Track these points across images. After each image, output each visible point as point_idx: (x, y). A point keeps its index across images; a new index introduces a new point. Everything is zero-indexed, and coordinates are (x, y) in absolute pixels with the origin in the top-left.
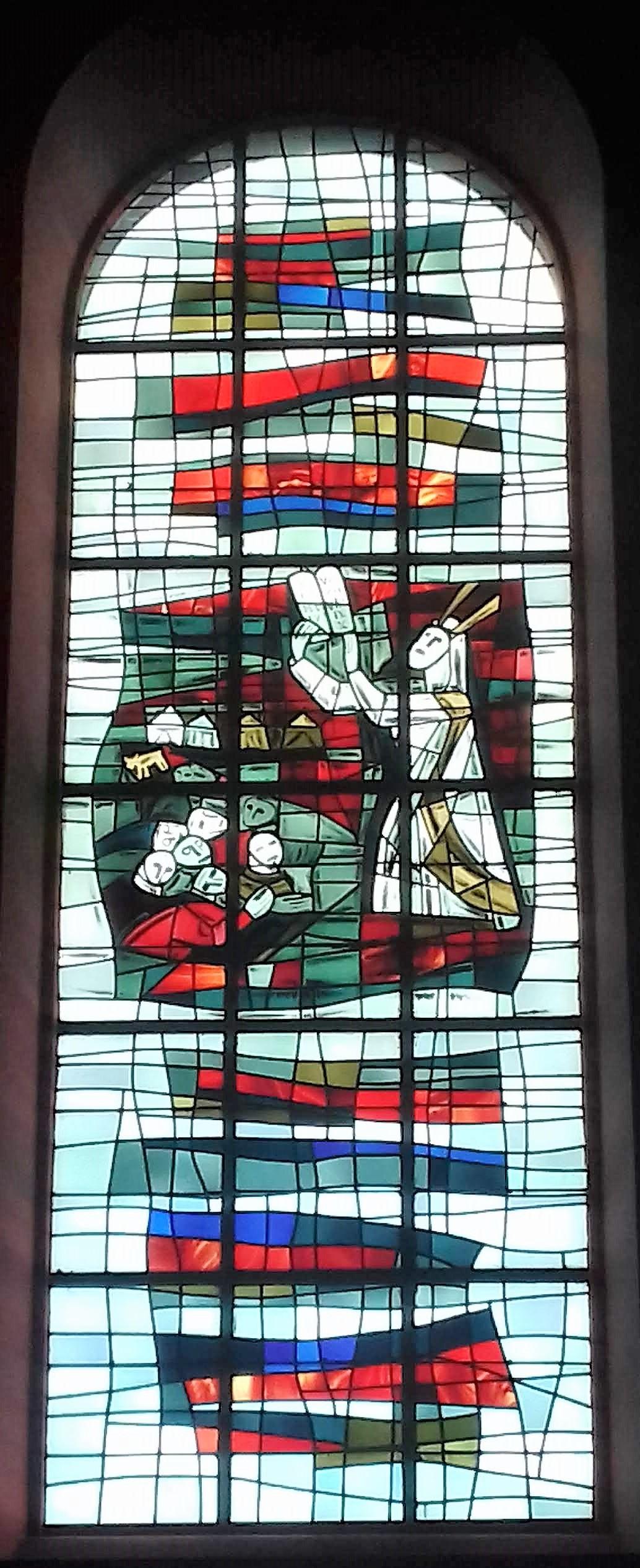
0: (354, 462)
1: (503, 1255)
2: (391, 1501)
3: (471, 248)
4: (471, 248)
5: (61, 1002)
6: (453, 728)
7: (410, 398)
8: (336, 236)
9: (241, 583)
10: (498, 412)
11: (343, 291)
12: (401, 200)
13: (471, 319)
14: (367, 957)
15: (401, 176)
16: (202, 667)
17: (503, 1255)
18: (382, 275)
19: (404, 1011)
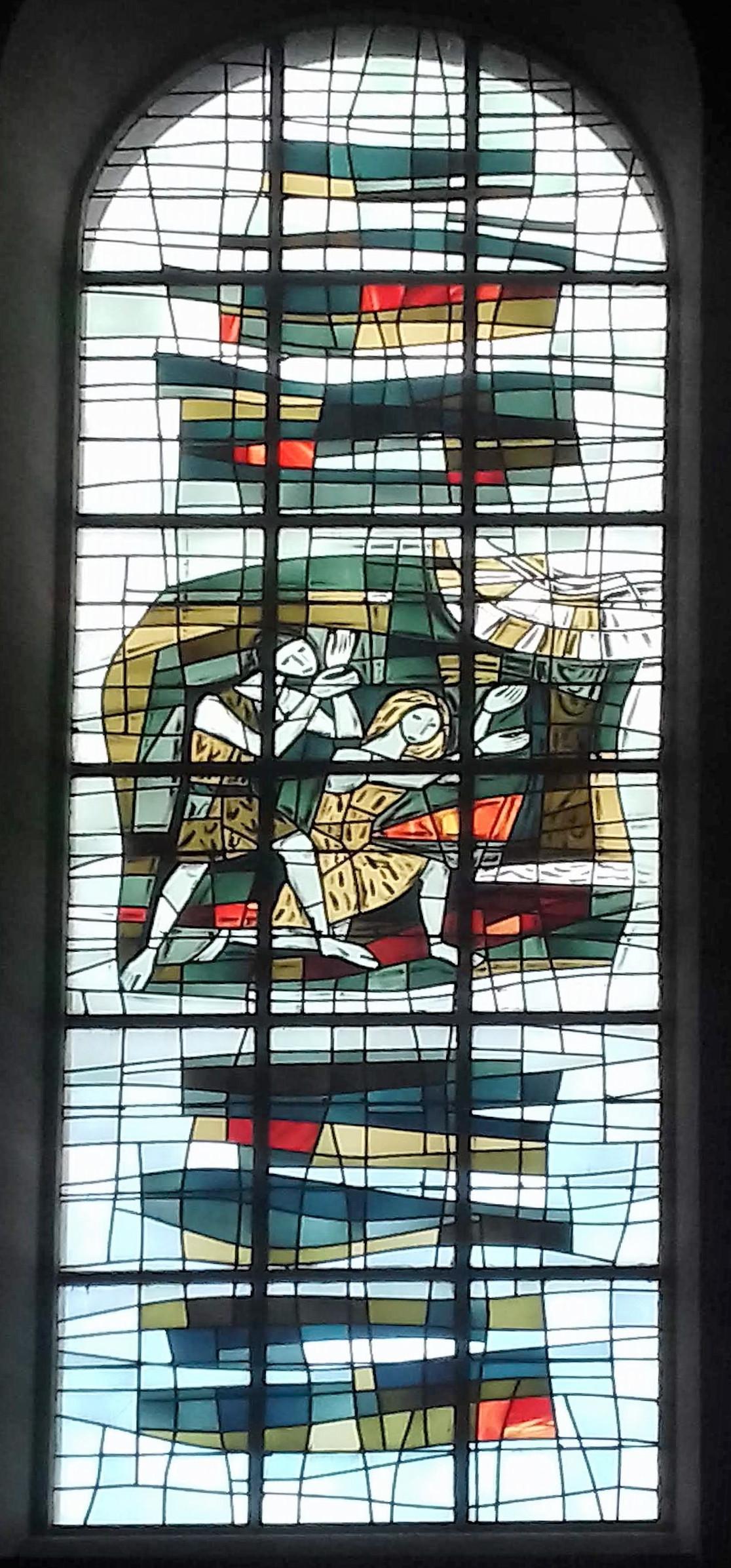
0: (303, 981)
1: (369, 74)
2: (523, 983)
3: (560, 1460)
4: (560, 1460)
5: (78, 608)
6: (570, 638)
7: (461, 268)
8: (374, 560)
9: (323, 404)
10: (535, 115)
11: (220, 1446)
12: (472, 116)
13: (571, 1252)
14: (236, 919)
15: (472, 93)
16: (222, 593)
17: (369, 74)
18: (315, 1390)
19: (474, 100)
